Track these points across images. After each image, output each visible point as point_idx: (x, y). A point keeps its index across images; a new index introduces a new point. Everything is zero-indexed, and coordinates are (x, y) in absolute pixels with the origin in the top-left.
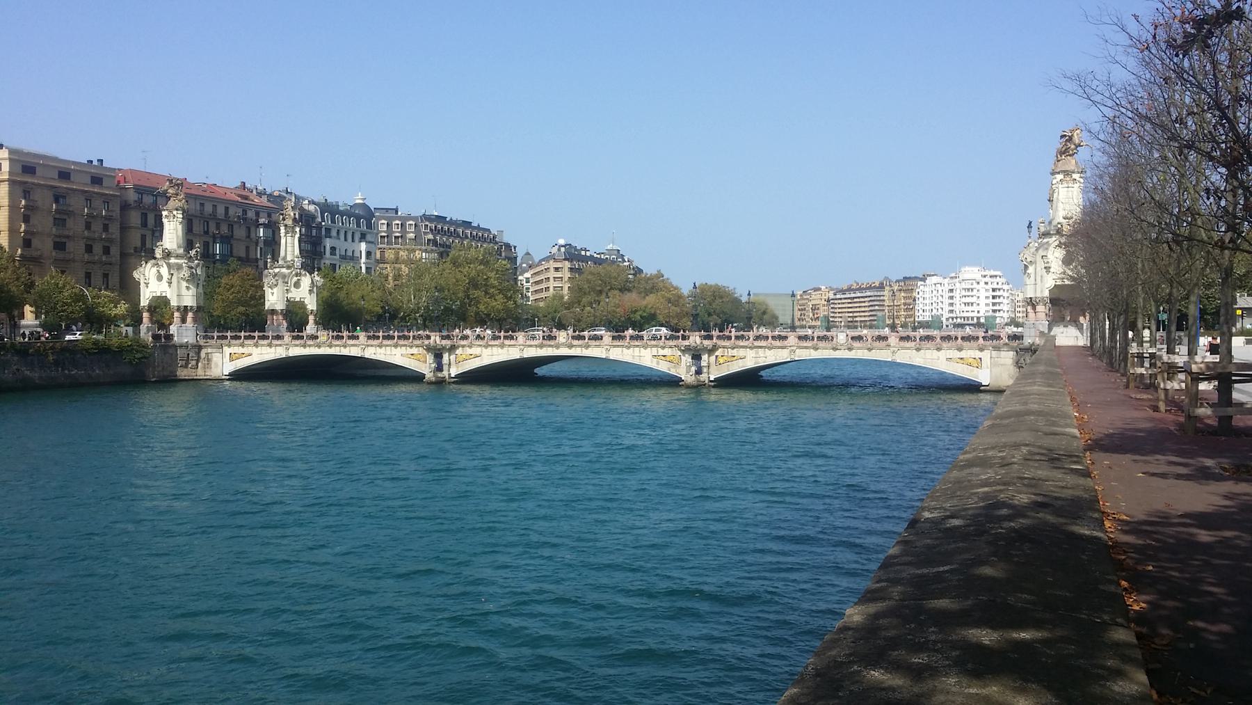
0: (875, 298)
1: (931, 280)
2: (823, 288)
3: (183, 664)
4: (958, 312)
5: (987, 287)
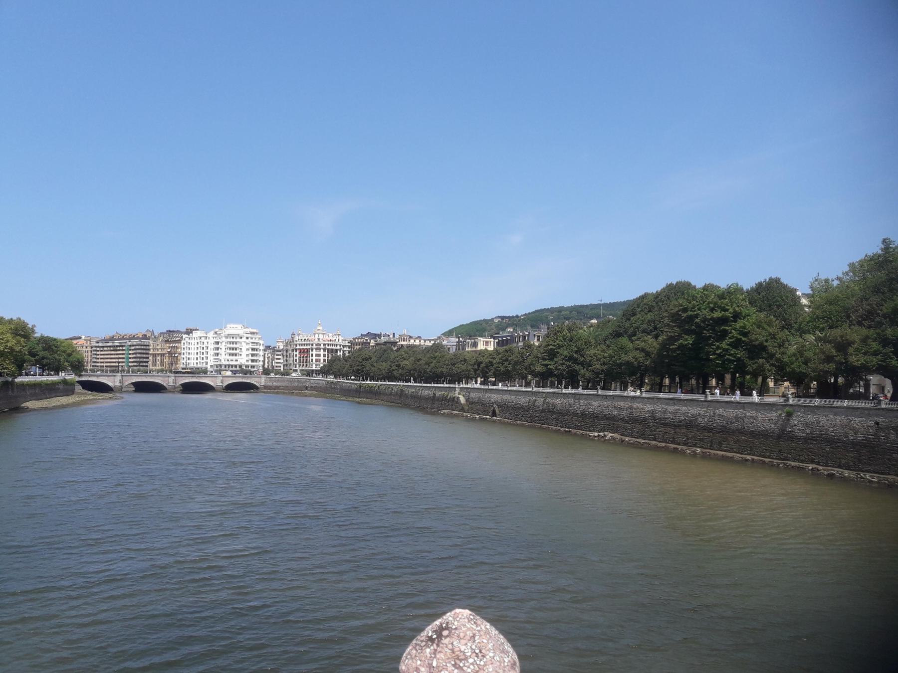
0: (139, 347)
1: (196, 334)
2: (83, 337)
3: (756, 631)
4: (223, 361)
5: (248, 341)
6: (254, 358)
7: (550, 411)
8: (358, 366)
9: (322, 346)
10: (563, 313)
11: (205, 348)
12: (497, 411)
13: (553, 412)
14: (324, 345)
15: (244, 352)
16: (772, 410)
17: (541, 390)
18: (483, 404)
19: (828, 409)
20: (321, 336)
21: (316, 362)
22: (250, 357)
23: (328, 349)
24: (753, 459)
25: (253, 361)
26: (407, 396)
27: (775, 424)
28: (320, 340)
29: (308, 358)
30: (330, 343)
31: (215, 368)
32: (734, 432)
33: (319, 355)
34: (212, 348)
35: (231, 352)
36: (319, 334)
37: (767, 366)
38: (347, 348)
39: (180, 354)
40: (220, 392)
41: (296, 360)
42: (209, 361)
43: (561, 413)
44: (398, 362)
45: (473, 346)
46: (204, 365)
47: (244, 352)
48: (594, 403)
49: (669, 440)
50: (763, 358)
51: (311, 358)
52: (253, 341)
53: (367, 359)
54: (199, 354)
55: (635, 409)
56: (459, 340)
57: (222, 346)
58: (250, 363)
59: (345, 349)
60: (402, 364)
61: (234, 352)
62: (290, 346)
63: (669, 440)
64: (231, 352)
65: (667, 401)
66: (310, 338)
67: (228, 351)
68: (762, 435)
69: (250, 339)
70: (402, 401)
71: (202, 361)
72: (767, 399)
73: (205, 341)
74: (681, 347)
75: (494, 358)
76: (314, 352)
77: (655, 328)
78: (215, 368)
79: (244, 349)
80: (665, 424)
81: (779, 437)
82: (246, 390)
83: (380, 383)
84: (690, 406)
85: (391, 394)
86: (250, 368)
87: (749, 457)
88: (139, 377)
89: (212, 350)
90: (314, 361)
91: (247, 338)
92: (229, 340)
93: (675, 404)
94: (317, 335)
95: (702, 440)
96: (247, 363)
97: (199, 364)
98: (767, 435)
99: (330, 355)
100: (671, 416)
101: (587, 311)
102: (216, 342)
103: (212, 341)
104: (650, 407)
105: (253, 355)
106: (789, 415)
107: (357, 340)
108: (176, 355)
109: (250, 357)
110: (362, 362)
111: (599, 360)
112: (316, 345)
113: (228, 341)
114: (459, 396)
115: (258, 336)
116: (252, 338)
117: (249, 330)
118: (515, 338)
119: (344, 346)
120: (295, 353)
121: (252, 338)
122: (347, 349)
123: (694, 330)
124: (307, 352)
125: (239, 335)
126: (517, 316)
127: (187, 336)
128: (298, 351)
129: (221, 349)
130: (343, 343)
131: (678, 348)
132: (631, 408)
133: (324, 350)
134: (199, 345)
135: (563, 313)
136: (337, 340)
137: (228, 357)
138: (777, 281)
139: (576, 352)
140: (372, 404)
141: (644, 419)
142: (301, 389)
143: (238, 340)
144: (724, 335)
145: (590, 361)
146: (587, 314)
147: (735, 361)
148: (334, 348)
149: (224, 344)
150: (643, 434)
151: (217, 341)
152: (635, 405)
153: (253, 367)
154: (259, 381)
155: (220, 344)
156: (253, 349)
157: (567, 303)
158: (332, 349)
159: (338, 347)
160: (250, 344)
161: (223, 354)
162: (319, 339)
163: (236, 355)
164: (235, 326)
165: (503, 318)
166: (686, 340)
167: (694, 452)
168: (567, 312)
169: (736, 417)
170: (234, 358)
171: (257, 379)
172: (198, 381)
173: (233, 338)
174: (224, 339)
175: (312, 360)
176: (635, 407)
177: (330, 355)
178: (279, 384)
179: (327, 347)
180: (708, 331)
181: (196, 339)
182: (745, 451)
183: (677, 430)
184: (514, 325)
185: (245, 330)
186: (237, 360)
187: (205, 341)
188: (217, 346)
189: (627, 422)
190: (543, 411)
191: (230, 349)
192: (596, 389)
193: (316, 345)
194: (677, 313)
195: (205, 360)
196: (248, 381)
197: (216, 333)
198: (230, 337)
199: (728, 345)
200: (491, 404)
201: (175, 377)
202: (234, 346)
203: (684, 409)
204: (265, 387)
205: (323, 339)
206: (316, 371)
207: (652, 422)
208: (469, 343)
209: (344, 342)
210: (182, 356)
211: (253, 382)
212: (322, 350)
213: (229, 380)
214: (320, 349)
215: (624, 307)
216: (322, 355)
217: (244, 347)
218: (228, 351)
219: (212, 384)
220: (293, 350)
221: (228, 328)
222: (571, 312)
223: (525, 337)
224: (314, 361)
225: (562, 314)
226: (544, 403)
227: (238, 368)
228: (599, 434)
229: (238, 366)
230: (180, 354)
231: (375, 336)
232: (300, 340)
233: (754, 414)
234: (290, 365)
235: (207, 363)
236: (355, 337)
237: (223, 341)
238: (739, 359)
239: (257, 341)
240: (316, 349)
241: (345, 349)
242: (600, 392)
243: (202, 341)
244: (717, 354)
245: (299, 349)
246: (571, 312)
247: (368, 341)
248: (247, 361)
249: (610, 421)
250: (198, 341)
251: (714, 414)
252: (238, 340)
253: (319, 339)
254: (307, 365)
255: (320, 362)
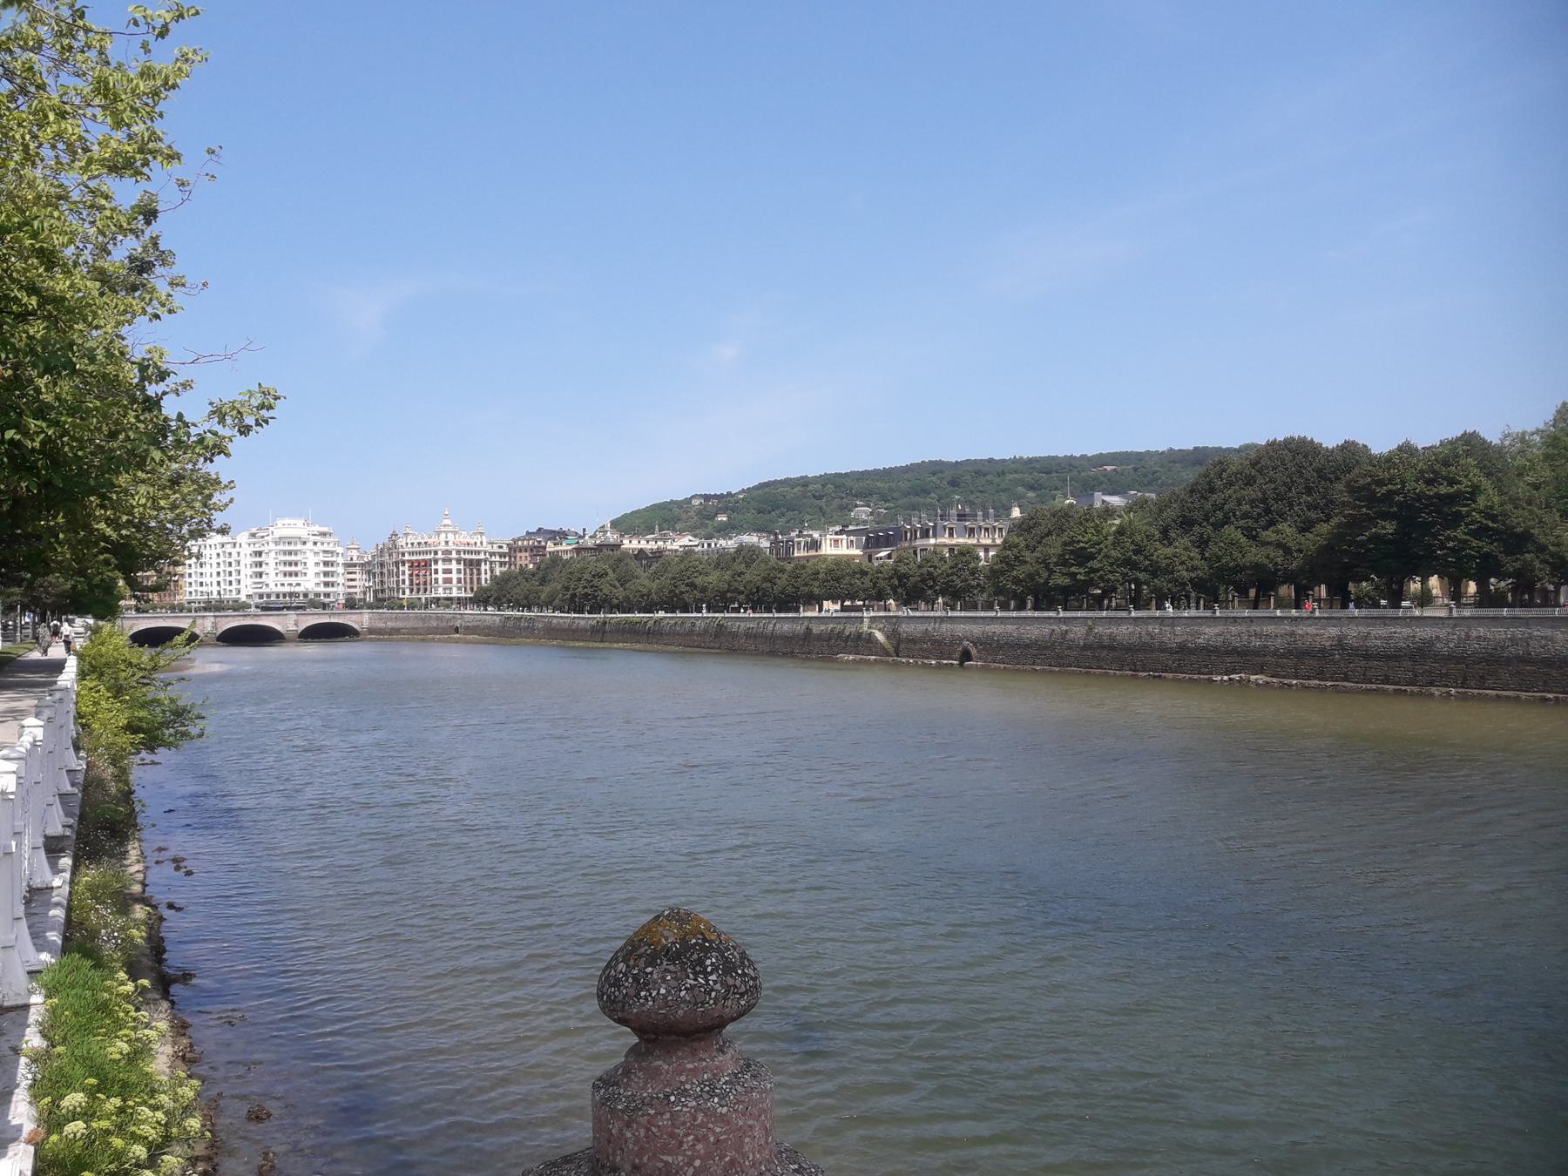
4: (272, 585)
5: (316, 549)
6: (329, 579)
7: (1103, 647)
9: (454, 555)
10: (811, 487)
11: (233, 564)
12: (974, 652)
13: (1111, 648)
14: (458, 552)
15: (312, 570)
19: (1430, 622)
20: (451, 537)
22: (323, 579)
23: (465, 560)
24: (1557, 698)
25: (327, 584)
26: (735, 635)
28: (450, 543)
29: (428, 578)
31: (258, 600)
32: (1508, 661)
33: (449, 571)
35: (288, 569)
36: (446, 532)
37: (1537, 564)
38: (497, 557)
39: (182, 575)
41: (404, 581)
42: (242, 586)
43: (1130, 649)
45: (811, 548)
46: (234, 595)
47: (312, 570)
48: (1207, 630)
49: (1377, 679)
50: (1528, 552)
52: (326, 547)
53: (600, 576)
56: (776, 538)
57: (270, 559)
58: (322, 589)
59: (493, 559)
60: (699, 581)
61: (293, 568)
63: (1377, 679)
64: (288, 569)
65: (1370, 621)
66: (430, 541)
67: (282, 568)
69: (319, 544)
70: (723, 644)
73: (234, 551)
74: (1376, 538)
75: (935, 567)
76: (440, 566)
77: (1268, 511)
79: (310, 564)
80: (1367, 656)
82: (337, 637)
84: (1417, 627)
87: (1551, 696)
88: (151, 621)
89: (248, 566)
90: (440, 581)
92: (281, 547)
94: (443, 536)
96: (318, 589)
97: (194, 594)
100: (1378, 642)
101: (851, 484)
103: (247, 550)
104: (1334, 631)
105: (326, 574)
107: (520, 543)
108: (176, 578)
109: (323, 579)
111: (1182, 563)
112: (443, 553)
115: (332, 539)
116: (322, 544)
117: (317, 529)
118: (906, 533)
119: (492, 554)
120: (401, 568)
121: (322, 544)
122: (497, 558)
123: (1395, 512)
124: (425, 565)
128: (407, 565)
129: (267, 564)
130: (489, 548)
131: (1370, 540)
132: (1292, 634)
133: (458, 561)
135: (811, 487)
136: (478, 544)
137: (281, 578)
138: (1474, 435)
139: (1136, 552)
140: (646, 651)
141: (1323, 650)
142: (444, 631)
143: (299, 547)
146: (851, 489)
148: (474, 557)
149: (272, 555)
152: (1300, 630)
153: (327, 595)
154: (359, 620)
155: (263, 555)
158: (471, 560)
159: (482, 556)
160: (321, 554)
161: (272, 574)
162: (447, 543)
163: (296, 575)
164: (292, 522)
165: (707, 497)
167: (1448, 693)
169: (1512, 639)
170: (293, 580)
174: (272, 546)
175: (436, 579)
176: (1300, 632)
178: (399, 624)
179: (462, 556)
181: (213, 547)
186: (298, 585)
187: (234, 551)
190: (1086, 647)
191: (285, 563)
192: (1056, 610)
193: (443, 553)
194: (1366, 487)
196: (341, 621)
197: (253, 535)
198: (284, 543)
199: (1466, 534)
200: (958, 640)
201: (215, 616)
202: (293, 558)
203: (1406, 631)
204: (371, 631)
205: (457, 540)
206: (459, 599)
208: (799, 543)
210: (188, 580)
211: (349, 623)
212: (454, 562)
214: (450, 560)
215: (1190, 475)
216: (454, 571)
217: (311, 560)
218: (282, 568)
219: (278, 628)
222: (824, 486)
224: (440, 581)
226: (1087, 634)
228: (1232, 676)
230: (182, 575)
231: (560, 535)
232: (409, 545)
233: (1549, 632)
234: (391, 589)
236: (516, 537)
239: (330, 548)
240: (444, 560)
241: (493, 559)
242: (1062, 614)
244: (1449, 548)
245: (409, 561)
246: (824, 486)
247: (543, 544)
248: (317, 584)
251: (1468, 637)
252: (299, 547)
253: (447, 543)
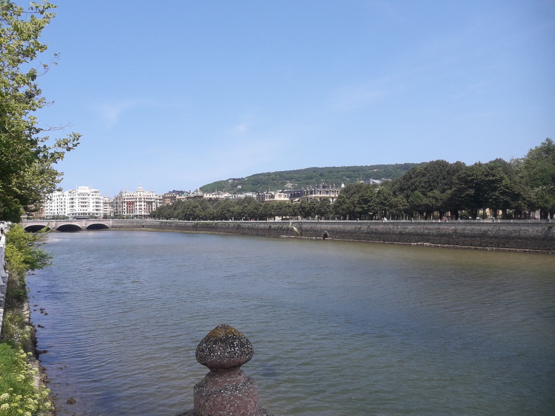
4: (77, 210)
5: (93, 197)
7: (373, 233)
8: (190, 211)
9: (143, 200)
10: (271, 176)
12: (328, 234)
13: (376, 233)
14: (144, 199)
15: (91, 205)
16: (539, 226)
17: (395, 221)
18: (315, 231)
20: (142, 193)
21: (139, 210)
22: (95, 208)
23: (147, 201)
25: (97, 210)
26: (244, 228)
27: (541, 233)
30: (147, 197)
31: (72, 216)
32: (513, 238)
34: (68, 202)
35: (83, 204)
36: (140, 191)
37: (523, 204)
39: (44, 207)
40: (85, 230)
41: (125, 209)
42: (66, 211)
43: (382, 234)
44: (227, 208)
45: (271, 198)
46: (63, 214)
47: (91, 205)
48: (409, 227)
50: (520, 200)
51: (135, 207)
52: (96, 197)
54: (59, 206)
55: (442, 229)
56: (259, 194)
57: (76, 201)
58: (95, 212)
59: (157, 201)
60: (231, 209)
61: (85, 204)
62: (120, 200)
64: (83, 204)
66: (134, 195)
68: (532, 239)
69: (94, 196)
70: (240, 231)
71: (61, 211)
72: (485, 221)
73: (63, 198)
76: (138, 204)
78: (72, 216)
79: (91, 203)
81: (544, 239)
83: (216, 221)
85: (228, 228)
86: (95, 215)
87: (527, 250)
89: (68, 203)
90: (138, 209)
91: (93, 195)
92: (80, 197)
93: (471, 225)
95: (490, 243)
96: (93, 212)
98: (535, 239)
99: (148, 205)
102: (71, 199)
103: (68, 198)
105: (97, 206)
106: (550, 228)
107: (167, 195)
108: (42, 207)
109: (95, 208)
110: (192, 209)
111: (400, 204)
112: (139, 199)
113: (80, 198)
114: (293, 227)
116: (95, 195)
117: (93, 190)
118: (304, 192)
119: (156, 199)
120: (124, 204)
121: (95, 195)
122: (159, 201)
124: (132, 203)
125: (87, 193)
126: (242, 178)
127: (48, 195)
128: (126, 203)
129: (75, 203)
130: (155, 197)
132: (439, 229)
133: (144, 202)
134: (59, 201)
135: (271, 176)
136: (152, 196)
137: (80, 208)
141: (449, 234)
142: (139, 227)
143: (87, 196)
144: (495, 189)
145: (395, 204)
146: (285, 177)
147: (502, 202)
148: (150, 200)
149: (77, 199)
150: (449, 242)
151: (72, 197)
153: (97, 214)
154: (108, 223)
155: (74, 199)
156: (97, 203)
157: (272, 170)
159: (153, 200)
160: (95, 199)
162: (140, 195)
163: (86, 206)
165: (234, 180)
166: (471, 192)
168: (274, 176)
170: (85, 208)
171: (107, 222)
172: (70, 224)
173: (83, 195)
174: (77, 196)
175: (136, 208)
176: (441, 228)
177: (148, 205)
179: (146, 200)
180: (486, 187)
181: (55, 196)
182: (521, 247)
183: (473, 239)
184: (241, 184)
185: (91, 190)
186: (87, 210)
187: (63, 198)
188: (72, 201)
189: (436, 236)
191: (82, 202)
192: (357, 220)
193: (139, 199)
195: (63, 210)
196: (102, 223)
198: (82, 195)
200: (322, 230)
201: (56, 221)
202: (85, 200)
203: (478, 228)
204: (113, 227)
206: (144, 215)
207: (455, 235)
209: (156, 196)
210: (46, 208)
211: (105, 224)
212: (143, 202)
213: (90, 223)
214: (141, 201)
215: (403, 173)
216: (143, 205)
217: (91, 201)
219: (79, 225)
220: (122, 203)
221: (80, 189)
222: (276, 176)
223: (308, 192)
224: (138, 209)
225: (270, 177)
226: (368, 228)
227: (88, 215)
229: (88, 214)
230: (44, 207)
232: (127, 196)
233: (527, 228)
235: (65, 213)
236: (165, 193)
237: (76, 198)
238: (506, 201)
239: (98, 197)
241: (157, 201)
243: (61, 198)
245: (126, 202)
246: (276, 176)
247: (175, 196)
248: (93, 210)
249: (423, 236)
250: (58, 198)
251: (499, 230)
252: (87, 196)
253: (140, 195)
254: (132, 212)
255: (142, 210)
